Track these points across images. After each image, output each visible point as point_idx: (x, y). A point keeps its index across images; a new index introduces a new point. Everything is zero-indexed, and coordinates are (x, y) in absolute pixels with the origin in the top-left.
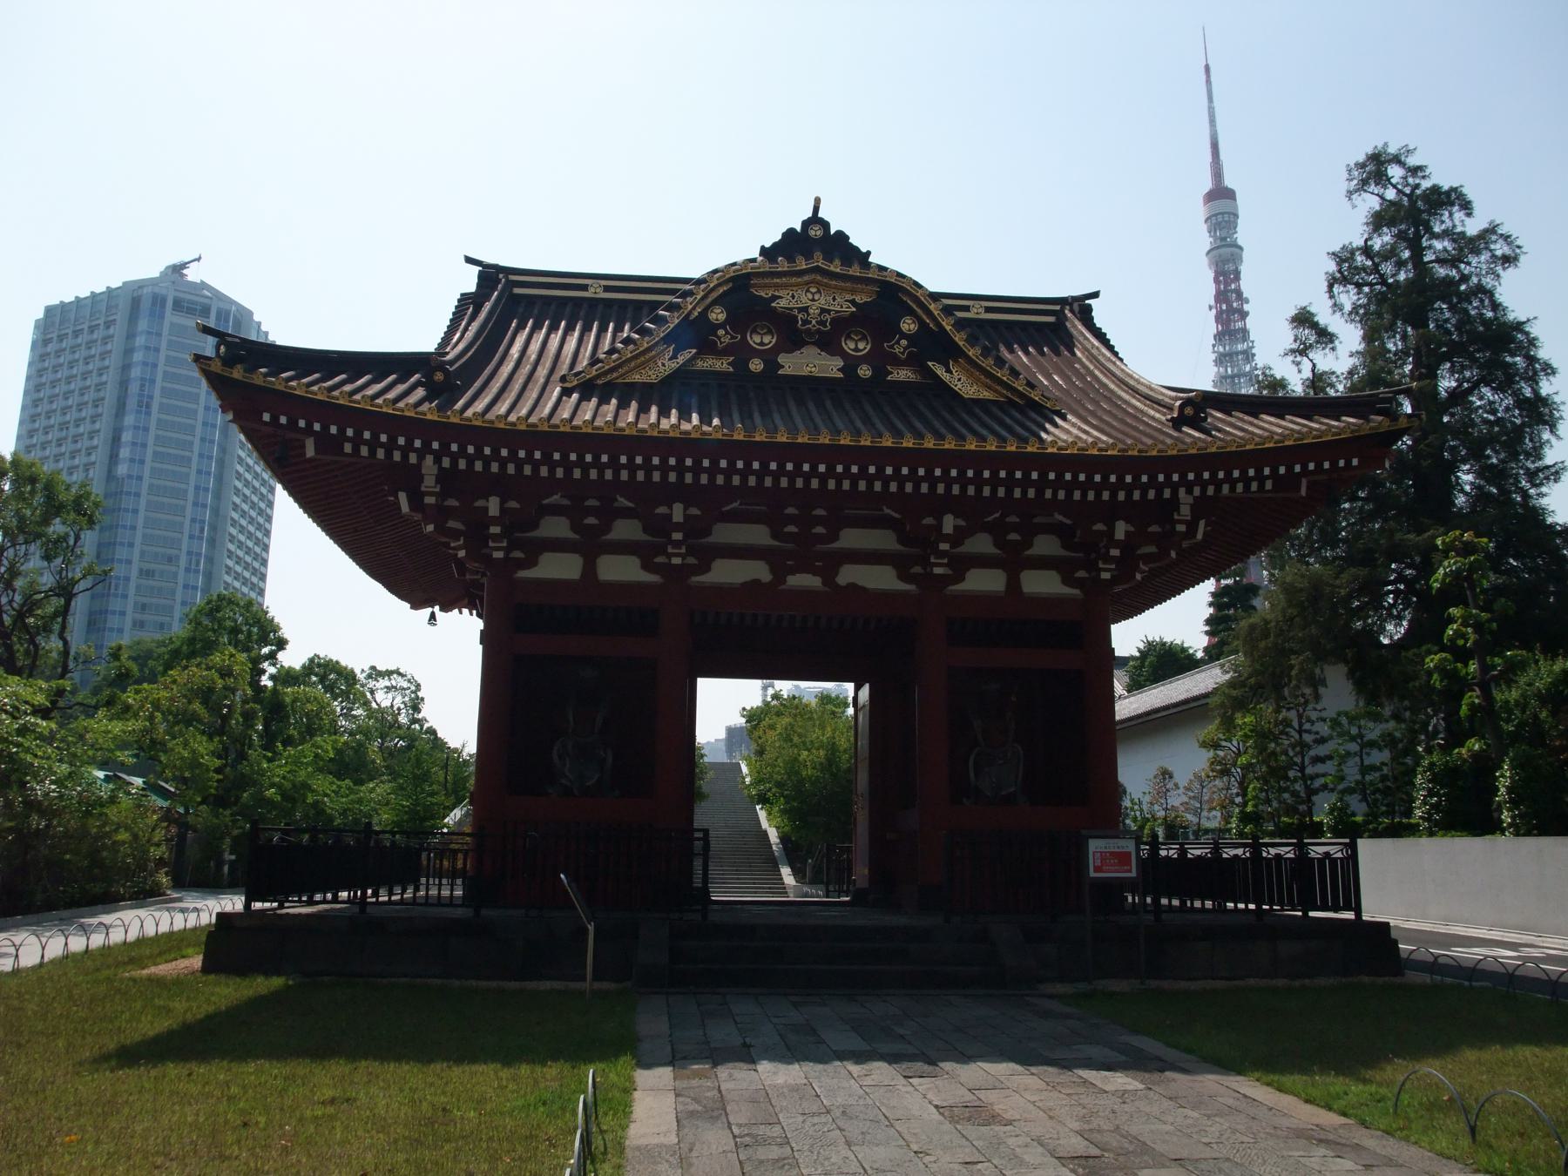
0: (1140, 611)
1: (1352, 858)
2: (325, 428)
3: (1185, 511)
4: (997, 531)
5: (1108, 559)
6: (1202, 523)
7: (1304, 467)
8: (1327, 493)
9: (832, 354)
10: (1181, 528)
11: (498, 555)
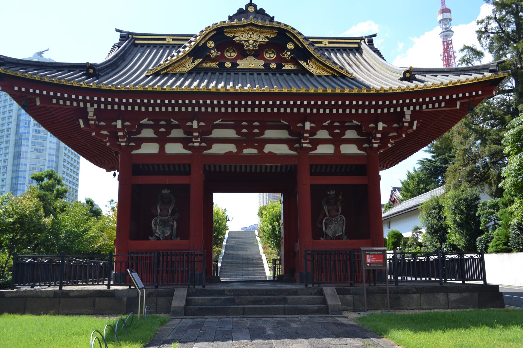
0: (397, 162)
1: (482, 259)
2: (41, 92)
3: (408, 117)
4: (330, 129)
5: (376, 138)
6: (416, 122)
7: (457, 95)
8: (468, 107)
9: (259, 59)
10: (406, 124)
11: (123, 144)
